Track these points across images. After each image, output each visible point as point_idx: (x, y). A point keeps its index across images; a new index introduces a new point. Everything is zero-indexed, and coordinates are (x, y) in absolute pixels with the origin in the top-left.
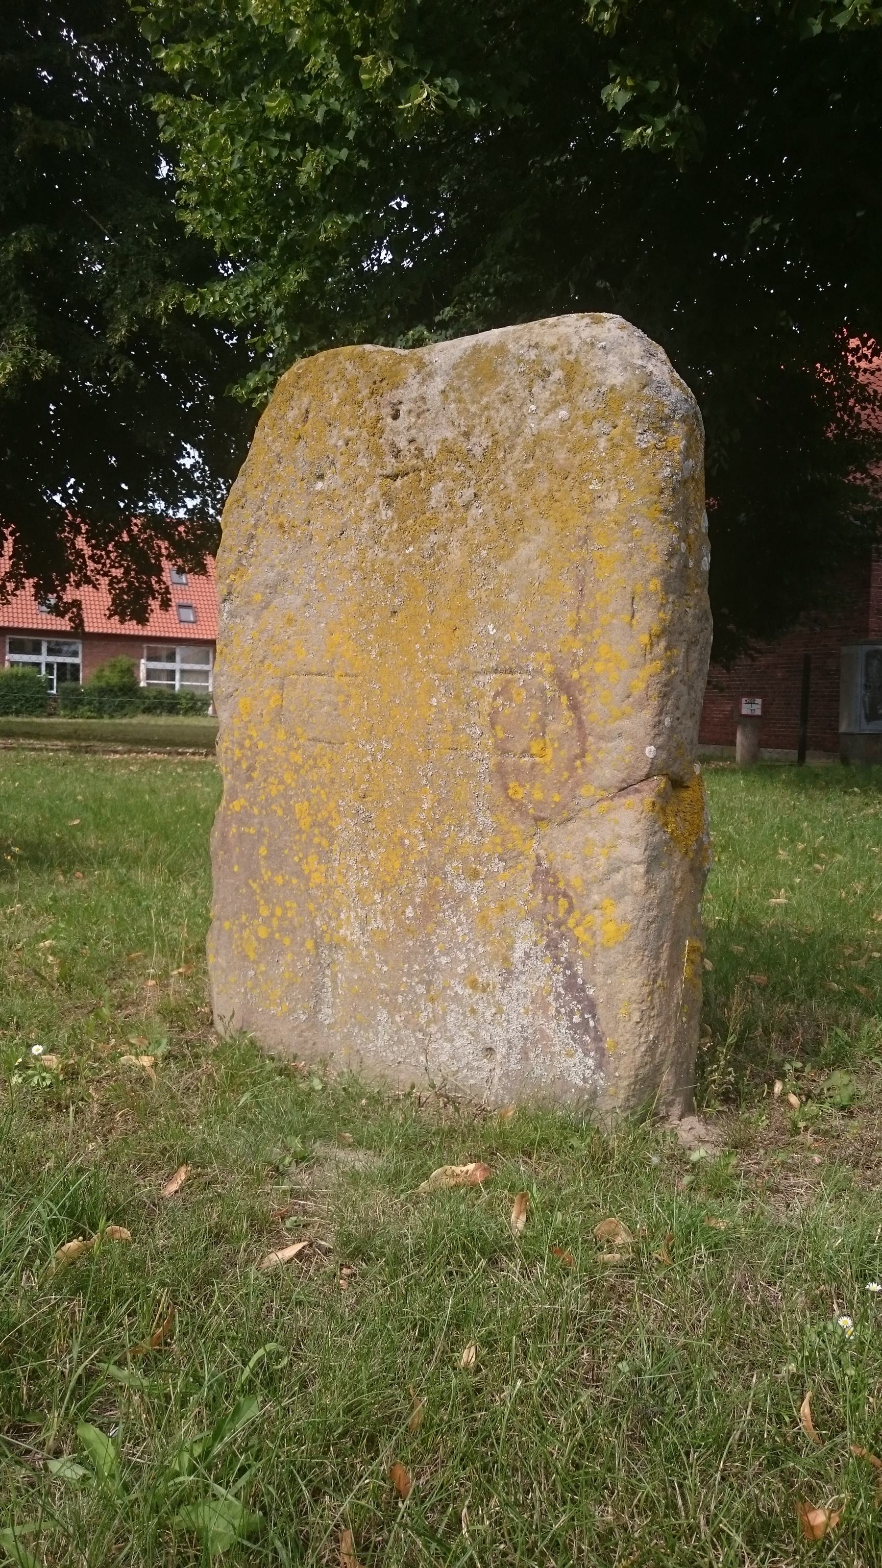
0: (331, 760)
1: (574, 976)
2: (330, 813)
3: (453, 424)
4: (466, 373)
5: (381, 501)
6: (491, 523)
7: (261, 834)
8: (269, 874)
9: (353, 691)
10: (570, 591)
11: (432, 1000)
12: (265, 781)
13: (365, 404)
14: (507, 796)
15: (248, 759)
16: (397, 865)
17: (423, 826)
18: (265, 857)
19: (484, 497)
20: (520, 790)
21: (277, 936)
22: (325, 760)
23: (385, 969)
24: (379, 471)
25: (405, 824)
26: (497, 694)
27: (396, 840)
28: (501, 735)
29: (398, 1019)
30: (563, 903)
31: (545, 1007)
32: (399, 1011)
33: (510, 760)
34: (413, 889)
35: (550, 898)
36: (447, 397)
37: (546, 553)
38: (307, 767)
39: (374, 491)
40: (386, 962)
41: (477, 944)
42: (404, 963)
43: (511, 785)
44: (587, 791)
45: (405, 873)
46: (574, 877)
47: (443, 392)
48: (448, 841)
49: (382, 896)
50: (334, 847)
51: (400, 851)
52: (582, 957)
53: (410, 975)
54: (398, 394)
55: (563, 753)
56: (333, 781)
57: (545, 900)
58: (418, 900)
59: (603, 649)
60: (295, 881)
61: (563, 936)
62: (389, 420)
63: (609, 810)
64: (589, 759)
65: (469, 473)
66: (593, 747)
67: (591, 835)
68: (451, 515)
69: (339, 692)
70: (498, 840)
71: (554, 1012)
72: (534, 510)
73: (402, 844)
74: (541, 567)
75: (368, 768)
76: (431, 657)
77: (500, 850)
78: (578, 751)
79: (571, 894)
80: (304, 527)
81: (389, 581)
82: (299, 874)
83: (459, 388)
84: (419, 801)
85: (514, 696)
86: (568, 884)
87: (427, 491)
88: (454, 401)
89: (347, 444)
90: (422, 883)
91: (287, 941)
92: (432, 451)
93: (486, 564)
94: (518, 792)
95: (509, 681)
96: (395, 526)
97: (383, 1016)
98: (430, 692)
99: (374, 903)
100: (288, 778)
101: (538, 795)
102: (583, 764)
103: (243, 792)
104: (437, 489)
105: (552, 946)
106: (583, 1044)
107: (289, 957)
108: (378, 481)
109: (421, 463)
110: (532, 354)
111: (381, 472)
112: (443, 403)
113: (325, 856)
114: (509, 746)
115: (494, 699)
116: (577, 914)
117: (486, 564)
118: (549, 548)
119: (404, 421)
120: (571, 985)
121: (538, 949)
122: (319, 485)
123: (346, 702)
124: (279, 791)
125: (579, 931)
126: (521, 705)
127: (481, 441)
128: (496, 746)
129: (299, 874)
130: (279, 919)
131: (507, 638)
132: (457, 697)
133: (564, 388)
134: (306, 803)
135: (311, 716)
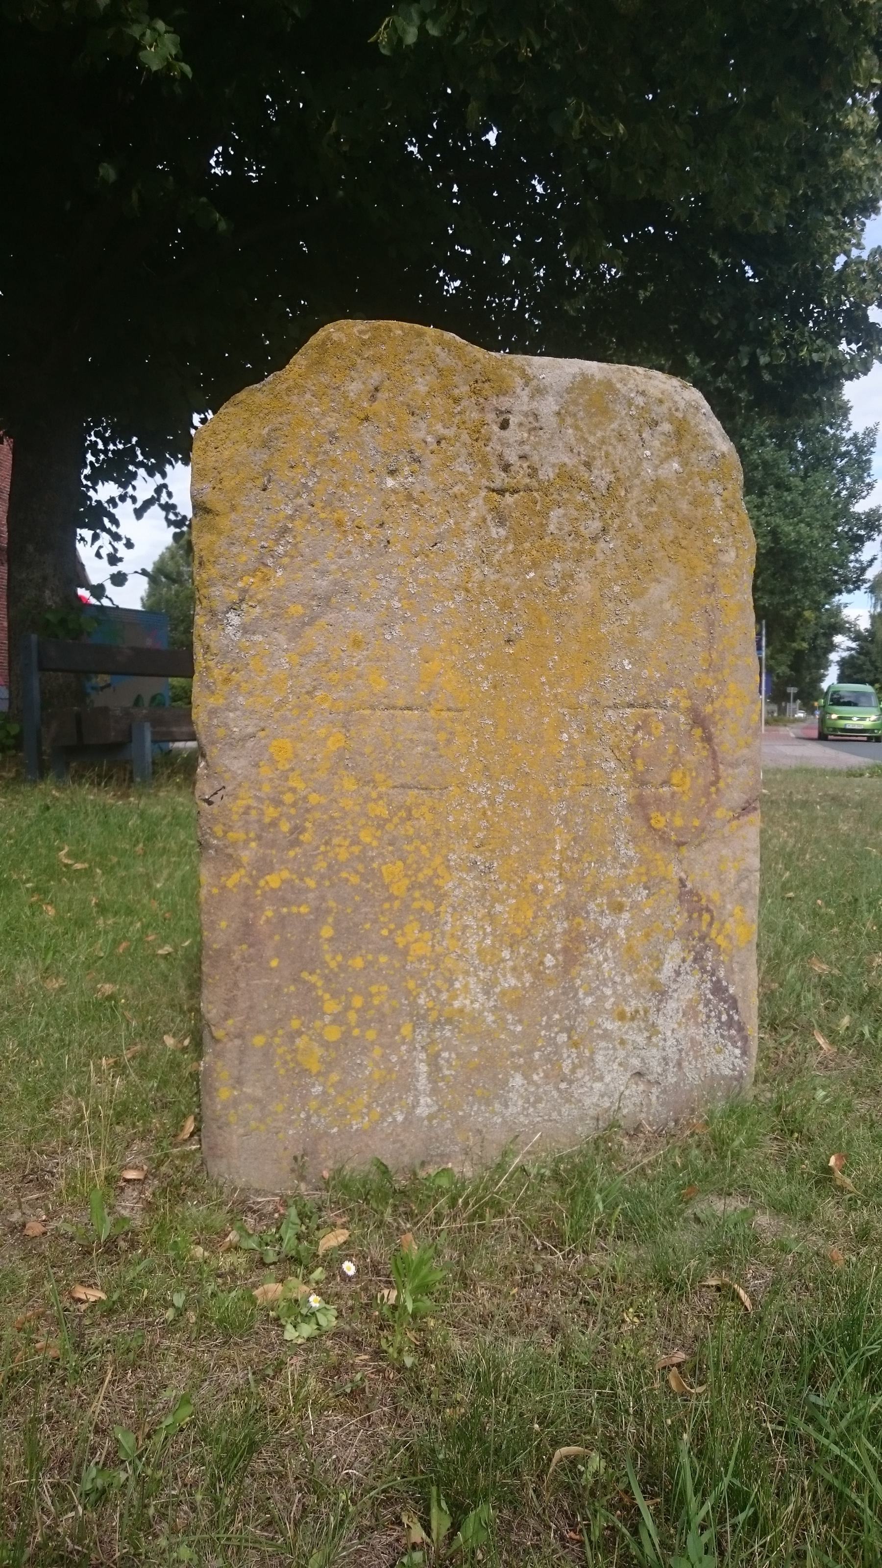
0: (432, 809)
1: (719, 981)
2: (435, 870)
3: (572, 451)
4: (581, 401)
5: (489, 517)
6: (621, 560)
7: (320, 913)
8: (339, 958)
9: (458, 728)
10: (702, 633)
11: (576, 1045)
12: (327, 843)
13: (464, 403)
14: (650, 827)
15: (290, 818)
16: (530, 914)
17: (561, 868)
18: (330, 940)
19: (612, 532)
20: (662, 819)
21: (356, 1032)
22: (424, 809)
23: (519, 1028)
24: (484, 482)
25: (538, 869)
26: (638, 728)
27: (527, 887)
28: (640, 768)
29: (535, 1077)
30: (706, 917)
31: (696, 1014)
32: (536, 1069)
33: (648, 791)
34: (551, 935)
35: (695, 915)
36: (563, 420)
37: (677, 596)
38: (396, 820)
39: (478, 505)
40: (520, 1021)
41: (623, 975)
42: (542, 1016)
43: (653, 815)
44: (720, 813)
45: (539, 921)
46: (712, 892)
47: (558, 414)
48: (589, 879)
49: (512, 952)
50: (442, 909)
51: (533, 898)
52: (723, 962)
53: (548, 1027)
54: (505, 402)
55: (700, 781)
56: (437, 834)
57: (690, 917)
58: (558, 946)
59: (732, 686)
60: (383, 959)
61: (706, 948)
62: (496, 428)
63: (740, 827)
64: (721, 784)
65: (592, 505)
66: (725, 774)
67: (724, 852)
68: (577, 545)
69: (439, 729)
70: (643, 870)
71: (704, 1018)
72: (662, 553)
73: (534, 890)
74: (672, 608)
75: (484, 814)
76: (560, 691)
77: (644, 879)
78: (713, 778)
79: (711, 907)
80: (375, 529)
81: (505, 605)
82: (392, 949)
83: (575, 415)
84: (551, 842)
85: (653, 730)
86: (709, 900)
87: (546, 516)
88: (571, 426)
89: (439, 442)
90: (561, 927)
91: (371, 1035)
92: (547, 473)
93: (617, 599)
94: (659, 821)
95: (647, 716)
96: (510, 547)
97: (518, 1080)
98: (560, 726)
99: (503, 960)
100: (366, 837)
101: (678, 822)
102: (718, 790)
103: (283, 862)
104: (555, 514)
105: (698, 958)
106: (731, 1038)
107: (377, 1052)
108: (483, 493)
109: (534, 484)
110: (640, 401)
111: (487, 484)
112: (559, 425)
113: (430, 922)
114: (648, 777)
115: (635, 732)
116: (716, 925)
117: (617, 599)
118: (680, 591)
119: (513, 434)
120: (718, 989)
121: (686, 964)
122: (390, 482)
123: (449, 742)
124: (351, 853)
125: (720, 940)
126: (658, 739)
127: (601, 476)
128: (635, 779)
129: (392, 949)
130: (358, 1011)
131: (645, 673)
132: (588, 732)
133: (674, 442)
134: (400, 864)
135: (398, 758)
